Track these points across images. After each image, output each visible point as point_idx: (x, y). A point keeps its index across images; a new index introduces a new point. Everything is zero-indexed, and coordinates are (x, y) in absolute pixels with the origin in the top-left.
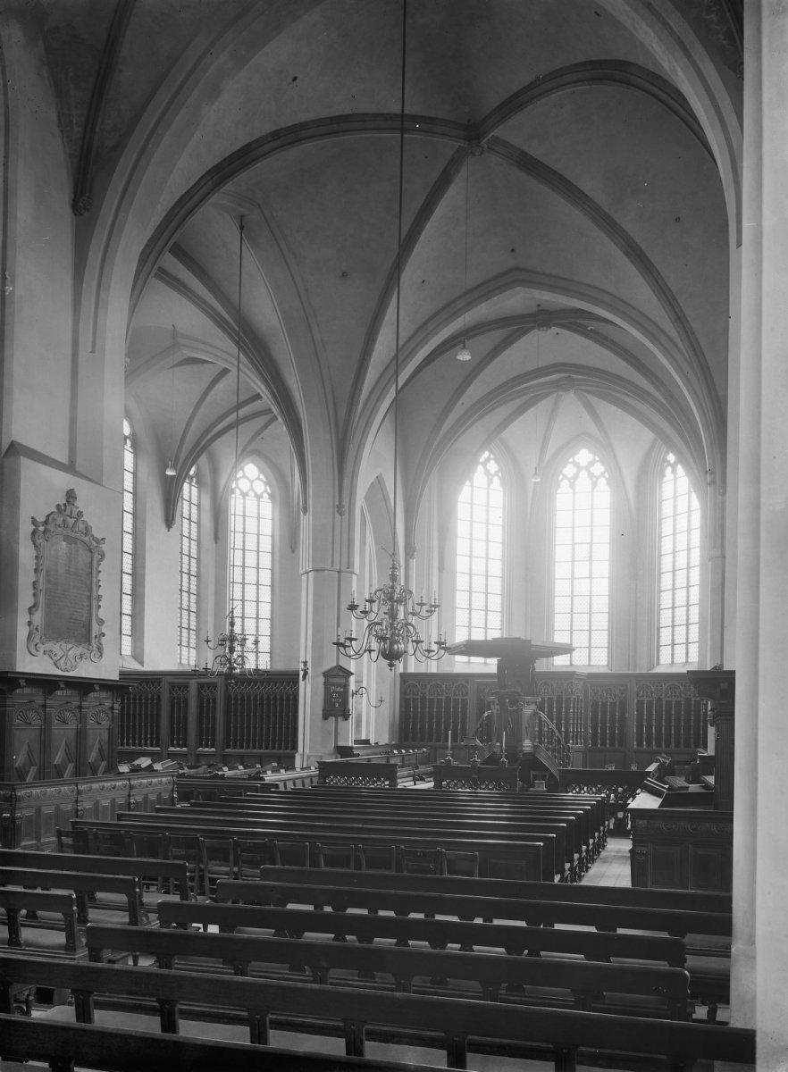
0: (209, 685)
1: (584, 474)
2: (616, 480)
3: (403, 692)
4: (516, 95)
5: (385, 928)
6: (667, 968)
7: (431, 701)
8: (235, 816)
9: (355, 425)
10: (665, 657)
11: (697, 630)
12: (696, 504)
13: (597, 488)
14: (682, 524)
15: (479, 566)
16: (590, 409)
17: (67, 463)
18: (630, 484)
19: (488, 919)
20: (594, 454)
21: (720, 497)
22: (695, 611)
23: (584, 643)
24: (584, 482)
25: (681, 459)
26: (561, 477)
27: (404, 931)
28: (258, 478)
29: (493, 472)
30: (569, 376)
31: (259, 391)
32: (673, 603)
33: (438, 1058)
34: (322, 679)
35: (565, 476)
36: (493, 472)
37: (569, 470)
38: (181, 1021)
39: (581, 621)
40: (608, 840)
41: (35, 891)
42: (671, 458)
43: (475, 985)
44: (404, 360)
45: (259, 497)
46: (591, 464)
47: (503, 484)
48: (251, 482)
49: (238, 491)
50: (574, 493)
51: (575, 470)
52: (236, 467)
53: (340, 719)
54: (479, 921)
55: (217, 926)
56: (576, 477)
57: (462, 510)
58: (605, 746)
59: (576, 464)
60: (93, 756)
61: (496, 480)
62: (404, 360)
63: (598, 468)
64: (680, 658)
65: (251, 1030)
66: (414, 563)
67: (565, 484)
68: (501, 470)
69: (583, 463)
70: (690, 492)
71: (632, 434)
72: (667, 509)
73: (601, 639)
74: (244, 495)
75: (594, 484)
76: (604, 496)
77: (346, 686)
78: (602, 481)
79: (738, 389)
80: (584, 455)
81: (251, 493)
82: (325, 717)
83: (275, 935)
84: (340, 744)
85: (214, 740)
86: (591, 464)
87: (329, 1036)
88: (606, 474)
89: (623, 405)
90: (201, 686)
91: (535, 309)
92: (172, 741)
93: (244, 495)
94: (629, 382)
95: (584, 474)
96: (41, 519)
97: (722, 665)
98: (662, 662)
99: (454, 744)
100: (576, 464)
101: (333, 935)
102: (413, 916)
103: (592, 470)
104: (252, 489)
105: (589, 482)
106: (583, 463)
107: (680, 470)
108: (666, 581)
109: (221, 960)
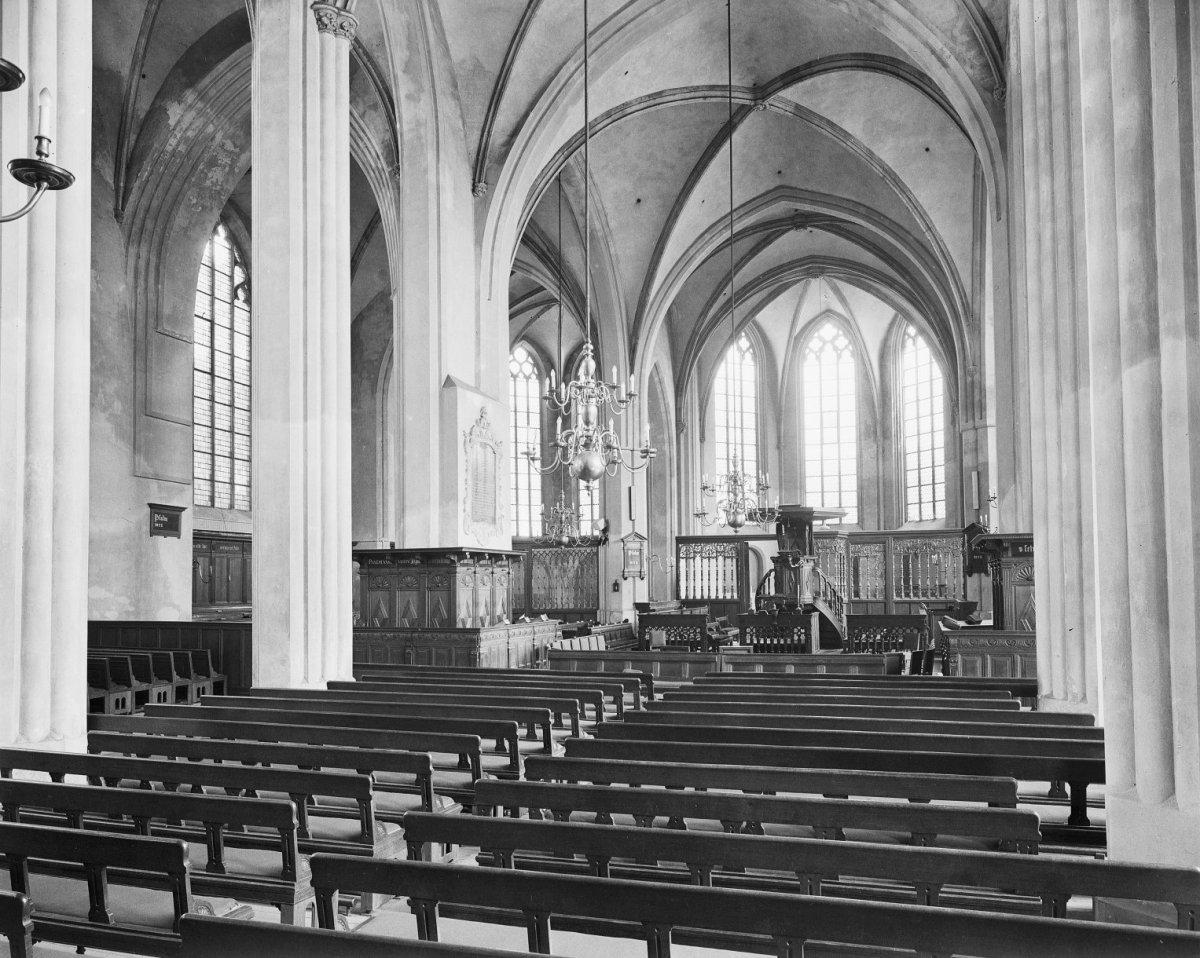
1: (829, 347)
5: (621, 802)
6: (721, 833)
8: (717, 691)
9: (647, 310)
10: (913, 513)
11: (943, 490)
13: (841, 360)
16: (837, 291)
19: (572, 781)
20: (839, 329)
24: (829, 354)
25: (921, 331)
26: (808, 350)
27: (604, 802)
28: (527, 361)
29: (744, 349)
30: (813, 265)
31: (542, 283)
32: (919, 465)
33: (515, 938)
35: (811, 350)
36: (744, 349)
38: (30, 875)
39: (831, 484)
41: (255, 767)
42: (912, 330)
45: (528, 378)
46: (835, 338)
48: (521, 364)
50: (820, 365)
53: (983, 574)
54: (689, 790)
55: (85, 777)
56: (821, 349)
57: (718, 385)
59: (821, 339)
63: (843, 342)
64: (927, 514)
65: (648, 944)
68: (752, 346)
69: (828, 337)
70: (931, 362)
75: (839, 357)
76: (849, 367)
79: (97, 368)
83: (597, 820)
84: (637, 601)
86: (835, 338)
87: (600, 934)
88: (851, 348)
89: (868, 289)
91: (793, 212)
95: (829, 347)
96: (468, 432)
97: (518, 535)
100: (821, 339)
101: (595, 814)
102: (583, 783)
103: (837, 343)
104: (521, 371)
105: (835, 354)
106: (828, 337)
107: (921, 341)
109: (165, 819)
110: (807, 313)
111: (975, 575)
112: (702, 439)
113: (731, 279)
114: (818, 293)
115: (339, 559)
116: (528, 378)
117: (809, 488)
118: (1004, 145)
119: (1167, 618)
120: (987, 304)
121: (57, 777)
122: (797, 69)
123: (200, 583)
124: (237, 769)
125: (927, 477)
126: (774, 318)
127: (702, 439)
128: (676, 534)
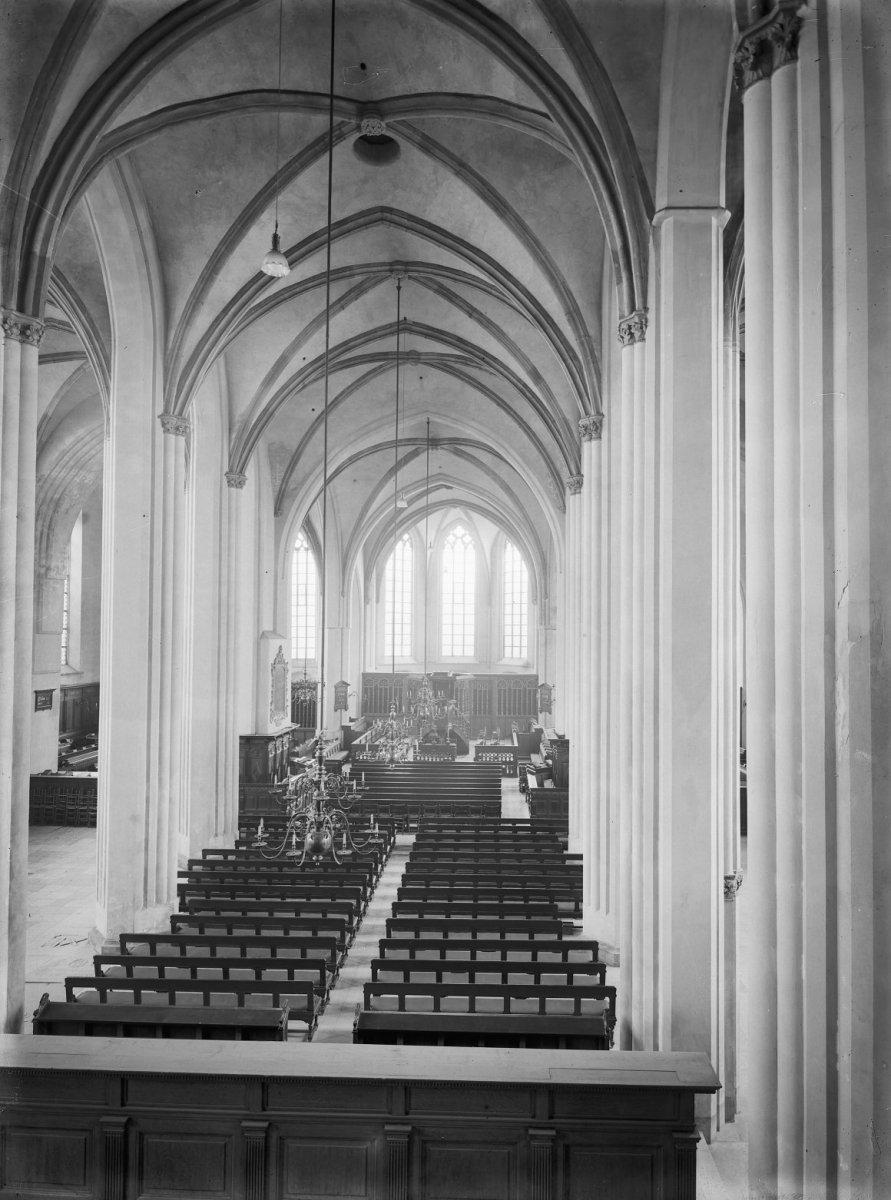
2: (479, 547)
3: (364, 684)
7: (381, 689)
12: (524, 566)
14: (517, 587)
17: (527, 815)
22: (525, 618)
34: (333, 689)
37: (451, 538)
43: (266, 881)
46: (464, 536)
51: (454, 539)
58: (658, 1050)
63: (468, 539)
66: (368, 606)
67: (448, 546)
71: (488, 529)
72: (508, 568)
75: (466, 548)
76: (472, 554)
77: (346, 692)
78: (471, 546)
80: (459, 530)
82: (336, 710)
84: (343, 724)
86: (464, 536)
94: (478, 443)
98: (506, 656)
105: (463, 547)
108: (508, 609)
110: (447, 521)
111: (543, 713)
112: (377, 601)
113: (330, 227)
114: (456, 512)
115: (234, 758)
117: (444, 622)
118: (564, 534)
119: (772, 517)
120: (571, 332)
121: (218, 913)
122: (458, 439)
123: (70, 712)
124: (253, 902)
125: (517, 600)
126: (429, 525)
127: (377, 601)
128: (362, 671)
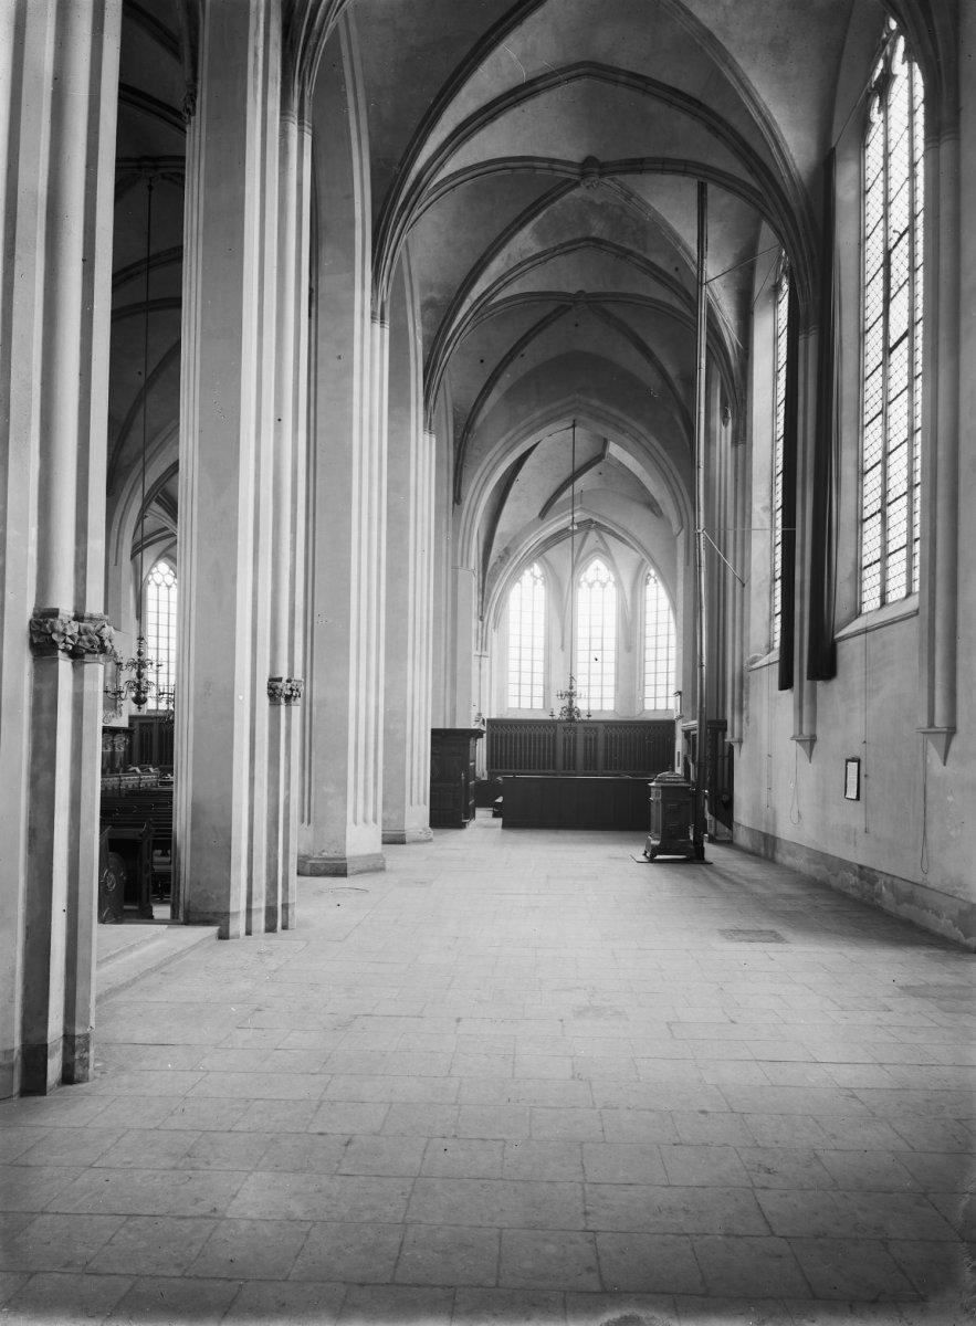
0: (147, 724)
2: (619, 583)
4: (642, 161)
15: (526, 642)
18: (627, 589)
21: (54, 604)
23: (599, 699)
40: (483, 815)
44: (151, 456)
45: (169, 587)
47: (544, 583)
49: (152, 583)
52: (154, 565)
60: (117, 765)
61: (540, 582)
62: (151, 456)
73: (610, 692)
74: (158, 585)
76: (611, 593)
81: (163, 584)
85: (151, 759)
90: (142, 725)
92: (142, 760)
93: (158, 585)
99: (114, 781)
116: (169, 587)
